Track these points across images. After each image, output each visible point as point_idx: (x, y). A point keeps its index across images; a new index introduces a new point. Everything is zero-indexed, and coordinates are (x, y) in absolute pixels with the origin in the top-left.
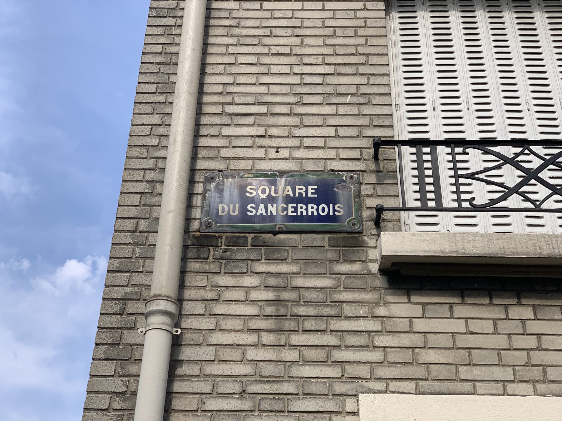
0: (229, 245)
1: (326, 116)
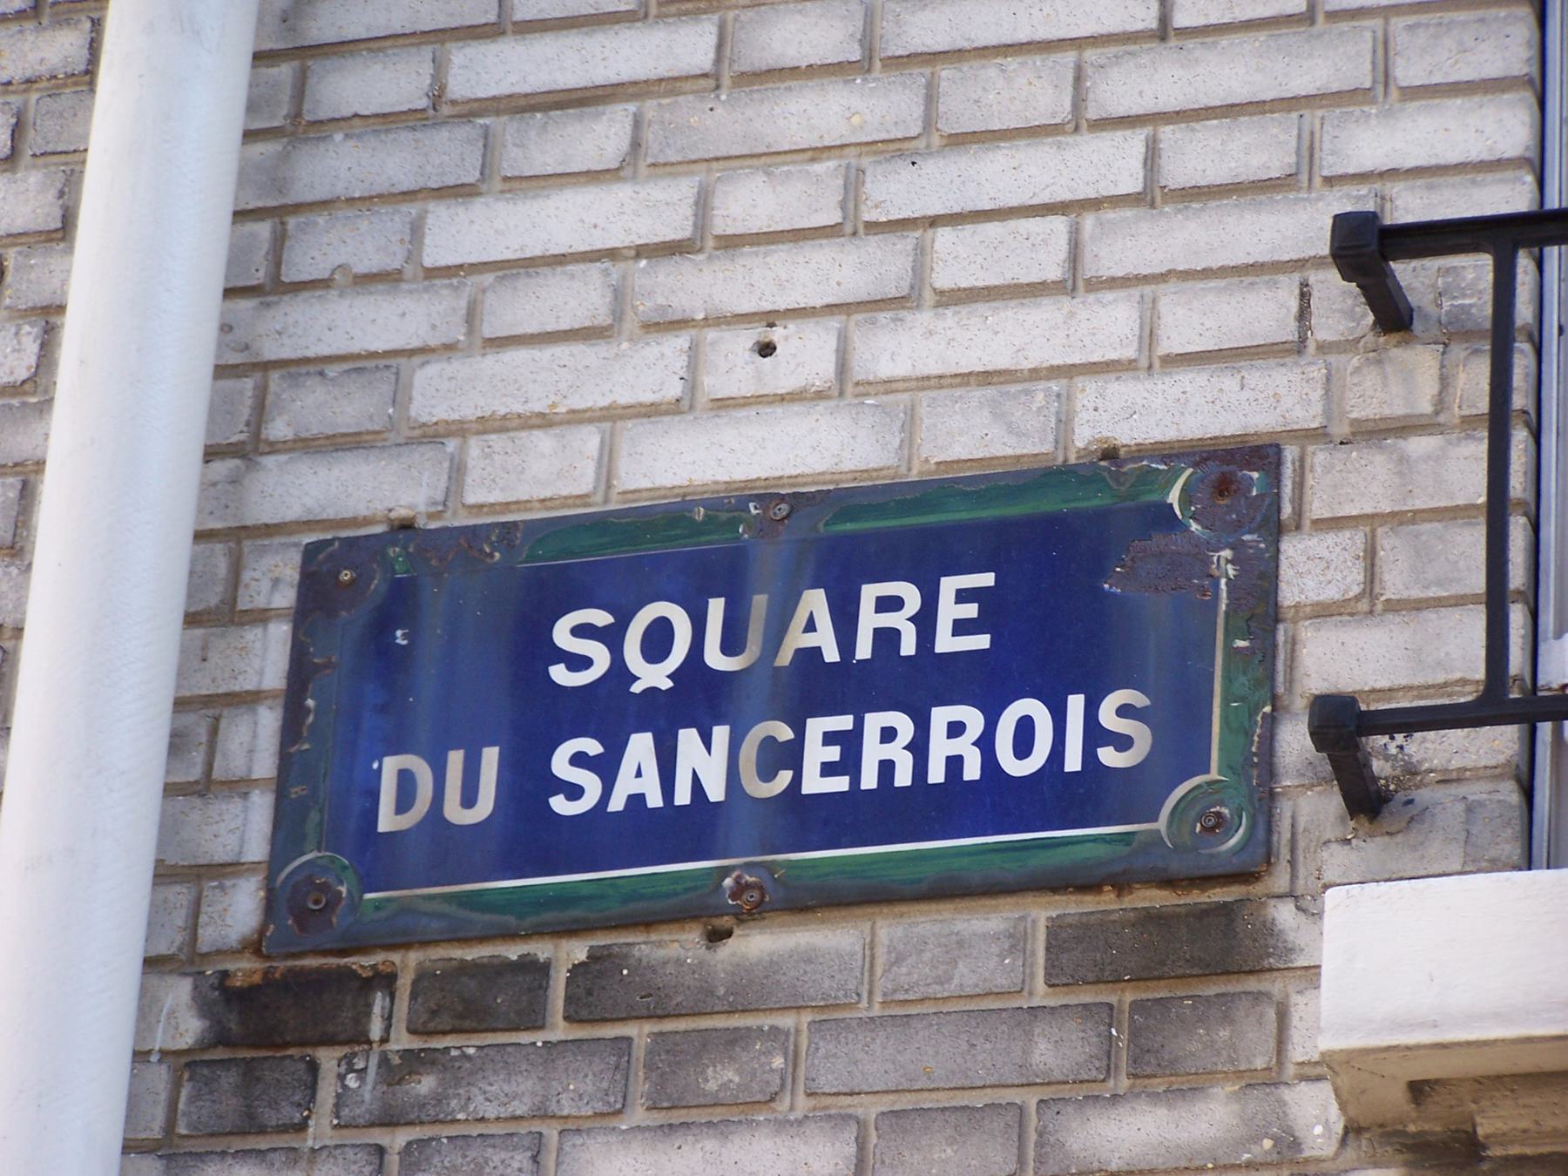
0: (431, 1026)
1: (1091, 55)
